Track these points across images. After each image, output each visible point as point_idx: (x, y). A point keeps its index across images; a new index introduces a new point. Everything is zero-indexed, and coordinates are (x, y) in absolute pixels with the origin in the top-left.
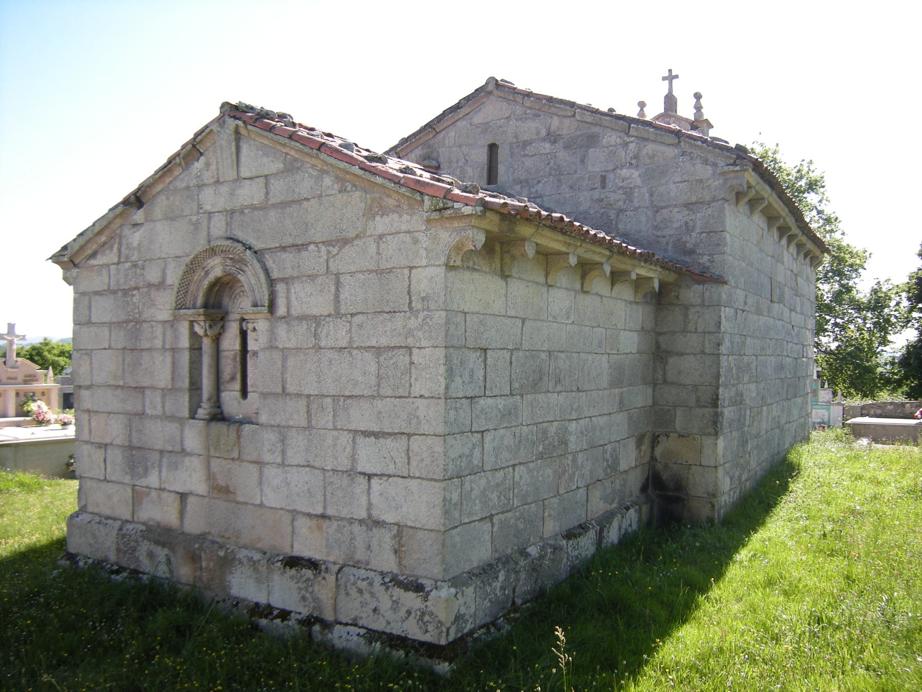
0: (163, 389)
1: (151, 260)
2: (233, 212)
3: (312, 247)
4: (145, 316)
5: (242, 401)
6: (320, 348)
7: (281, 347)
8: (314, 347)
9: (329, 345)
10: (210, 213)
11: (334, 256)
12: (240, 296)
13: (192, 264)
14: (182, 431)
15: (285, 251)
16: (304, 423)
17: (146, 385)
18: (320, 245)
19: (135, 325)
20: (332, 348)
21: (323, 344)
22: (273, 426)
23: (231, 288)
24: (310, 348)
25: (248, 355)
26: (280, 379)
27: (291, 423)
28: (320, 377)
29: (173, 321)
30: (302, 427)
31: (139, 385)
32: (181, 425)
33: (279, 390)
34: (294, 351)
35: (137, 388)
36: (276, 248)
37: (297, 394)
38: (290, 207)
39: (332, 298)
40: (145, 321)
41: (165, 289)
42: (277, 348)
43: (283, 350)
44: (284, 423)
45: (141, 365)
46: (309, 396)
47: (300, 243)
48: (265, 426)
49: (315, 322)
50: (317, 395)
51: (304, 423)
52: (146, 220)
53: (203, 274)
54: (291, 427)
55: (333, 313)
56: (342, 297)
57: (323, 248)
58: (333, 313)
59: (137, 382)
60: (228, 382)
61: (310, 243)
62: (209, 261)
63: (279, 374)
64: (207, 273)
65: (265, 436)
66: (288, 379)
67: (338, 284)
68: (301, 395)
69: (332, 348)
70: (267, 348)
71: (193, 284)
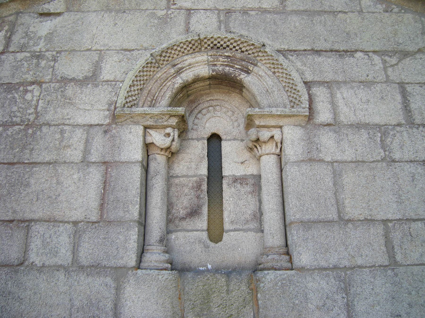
0: (75, 223)
1: (72, 51)
2: (229, 12)
3: (359, 55)
4: (49, 117)
5: (212, 244)
6: (394, 161)
7: (328, 159)
8: (383, 160)
9: (406, 158)
10: (189, 10)
11: (392, 66)
12: (208, 112)
13: (161, 56)
14: (118, 289)
15: (320, 55)
16: (384, 260)
17: (36, 216)
18: (371, 54)
19: (25, 130)
20: (411, 161)
21: (397, 156)
22: (325, 269)
23: (193, 102)
24: (378, 161)
25: (224, 182)
26: (333, 201)
27: (360, 262)
28: (400, 196)
29: (109, 125)
30: (380, 266)
31: (19, 216)
32: (117, 280)
33: (333, 215)
34: (353, 165)
35: (11, 221)
36: (305, 50)
37: (366, 219)
38: (320, 15)
39: (400, 106)
40: (48, 125)
41: (97, 86)
42: (321, 161)
43: (332, 163)
44: (346, 263)
45: (28, 185)
46: (385, 222)
47: (342, 49)
48: (308, 270)
49: (379, 132)
50: (400, 220)
51: (384, 260)
52: (68, 10)
53: (172, 71)
54: (360, 267)
55: (403, 122)
56: (413, 106)
57: (376, 59)
58: (403, 122)
59: (14, 212)
60: (183, 219)
61: (356, 51)
62: (186, 58)
63: (330, 194)
64: (179, 72)
65: (310, 285)
66: (347, 201)
67: (404, 94)
68: (372, 220)
69: (411, 161)
70: (303, 161)
71: (152, 82)
